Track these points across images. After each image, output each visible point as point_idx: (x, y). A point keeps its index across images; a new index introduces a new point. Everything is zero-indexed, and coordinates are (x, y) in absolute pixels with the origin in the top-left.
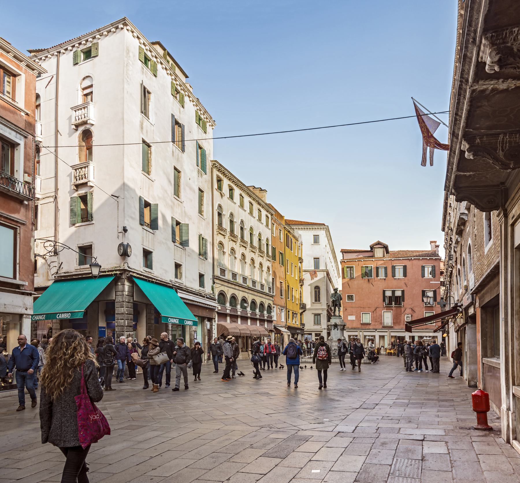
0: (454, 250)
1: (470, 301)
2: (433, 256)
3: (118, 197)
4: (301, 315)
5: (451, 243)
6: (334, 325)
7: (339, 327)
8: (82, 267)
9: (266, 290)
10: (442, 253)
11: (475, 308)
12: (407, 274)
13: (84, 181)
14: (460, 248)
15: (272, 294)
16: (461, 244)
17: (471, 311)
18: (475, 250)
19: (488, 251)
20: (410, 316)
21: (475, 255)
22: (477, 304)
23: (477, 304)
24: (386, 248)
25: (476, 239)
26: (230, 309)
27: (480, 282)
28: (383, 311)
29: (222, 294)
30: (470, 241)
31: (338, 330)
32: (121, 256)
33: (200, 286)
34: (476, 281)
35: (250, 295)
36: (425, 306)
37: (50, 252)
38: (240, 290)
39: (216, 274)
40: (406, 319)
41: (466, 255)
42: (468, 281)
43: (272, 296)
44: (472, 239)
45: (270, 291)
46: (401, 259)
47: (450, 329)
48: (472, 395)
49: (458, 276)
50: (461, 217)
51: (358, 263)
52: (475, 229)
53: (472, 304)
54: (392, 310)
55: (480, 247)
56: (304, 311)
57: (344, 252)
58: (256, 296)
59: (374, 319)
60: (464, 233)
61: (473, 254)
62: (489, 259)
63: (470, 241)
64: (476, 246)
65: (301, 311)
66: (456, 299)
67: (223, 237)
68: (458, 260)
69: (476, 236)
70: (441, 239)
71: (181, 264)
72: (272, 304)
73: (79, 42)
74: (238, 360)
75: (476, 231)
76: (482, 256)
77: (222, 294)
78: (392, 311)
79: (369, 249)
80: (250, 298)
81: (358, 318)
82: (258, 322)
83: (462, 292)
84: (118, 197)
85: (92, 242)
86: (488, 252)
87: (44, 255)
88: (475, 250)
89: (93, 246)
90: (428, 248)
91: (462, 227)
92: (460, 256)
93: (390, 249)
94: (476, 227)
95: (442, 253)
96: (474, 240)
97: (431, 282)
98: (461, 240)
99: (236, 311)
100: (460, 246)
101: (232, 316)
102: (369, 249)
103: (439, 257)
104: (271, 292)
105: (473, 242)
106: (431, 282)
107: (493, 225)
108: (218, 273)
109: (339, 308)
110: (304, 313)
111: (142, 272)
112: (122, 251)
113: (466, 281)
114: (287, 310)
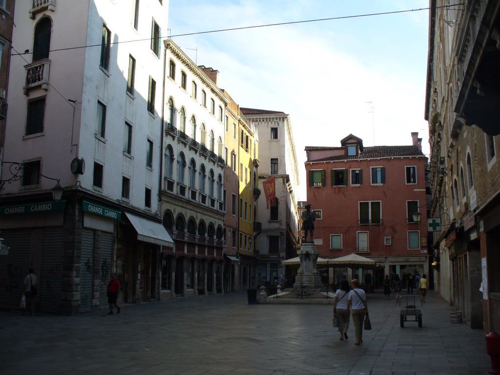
0: (448, 155)
1: (472, 224)
2: (415, 149)
3: (74, 102)
4: (255, 239)
5: (439, 139)
6: (305, 254)
7: (311, 257)
8: (27, 187)
9: (217, 206)
10: (426, 150)
11: (479, 233)
12: (386, 180)
13: (37, 84)
14: (456, 154)
15: (223, 211)
16: (457, 150)
17: (473, 236)
18: (476, 162)
19: (492, 168)
20: (390, 237)
21: (476, 169)
22: (482, 230)
23: (482, 230)
24: (359, 142)
25: (476, 150)
26: (199, 237)
27: (486, 204)
28: (357, 232)
29: (168, 214)
30: (468, 150)
31: (309, 260)
32: (73, 173)
33: (146, 205)
34: (479, 200)
35: (188, 211)
36: (408, 223)
37: (15, 176)
38: (188, 209)
39: (163, 188)
40: (385, 242)
41: (464, 166)
42: (468, 198)
43: (223, 215)
44: (471, 149)
45: (221, 208)
46: (379, 158)
47: (441, 255)
48: (487, 337)
49: (454, 189)
50: (457, 119)
51: (326, 165)
52: (475, 137)
53: (476, 227)
54: (369, 230)
55: (482, 162)
56: (258, 234)
57: (309, 150)
58: (205, 215)
59: (345, 243)
60: (460, 137)
61: (474, 167)
62: (494, 177)
63: (468, 150)
64: (477, 158)
65: (255, 234)
66: (452, 217)
67: (183, 146)
68: (453, 168)
69: (475, 146)
70: (424, 130)
71: (129, 178)
72: (222, 226)
73: (428, 225)
74: (358, 301)
75: (476, 141)
76: (484, 171)
77: (168, 214)
78: (368, 231)
79: (340, 146)
80: (198, 217)
81: (327, 241)
82: (215, 250)
83: (460, 210)
84: (74, 102)
85: (41, 158)
86: (491, 169)
87: (10, 180)
88: (476, 162)
89: (41, 162)
90: (409, 142)
91: (459, 131)
92: (456, 164)
93: (366, 144)
94: (475, 136)
95: (426, 150)
96: (474, 150)
97: (415, 190)
98: (456, 144)
99: (204, 240)
100: (456, 151)
101: (209, 247)
102: (340, 146)
103: (423, 154)
104: (222, 210)
105: (472, 151)
106: (415, 190)
107: (495, 141)
108: (164, 186)
109: (311, 232)
110: (258, 236)
111: (92, 192)
112: (76, 169)
113: (465, 198)
114: (240, 233)
